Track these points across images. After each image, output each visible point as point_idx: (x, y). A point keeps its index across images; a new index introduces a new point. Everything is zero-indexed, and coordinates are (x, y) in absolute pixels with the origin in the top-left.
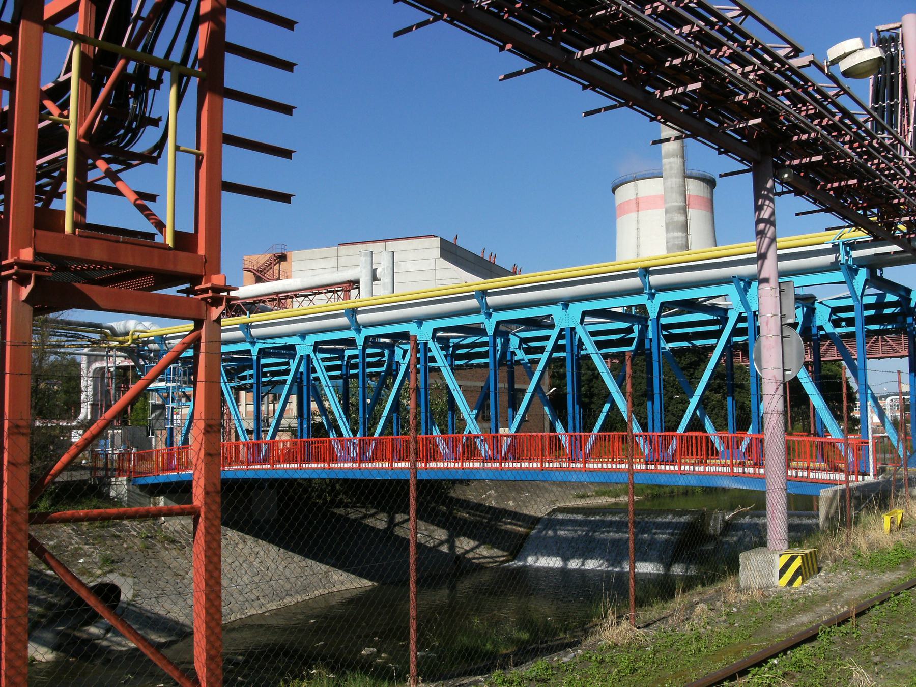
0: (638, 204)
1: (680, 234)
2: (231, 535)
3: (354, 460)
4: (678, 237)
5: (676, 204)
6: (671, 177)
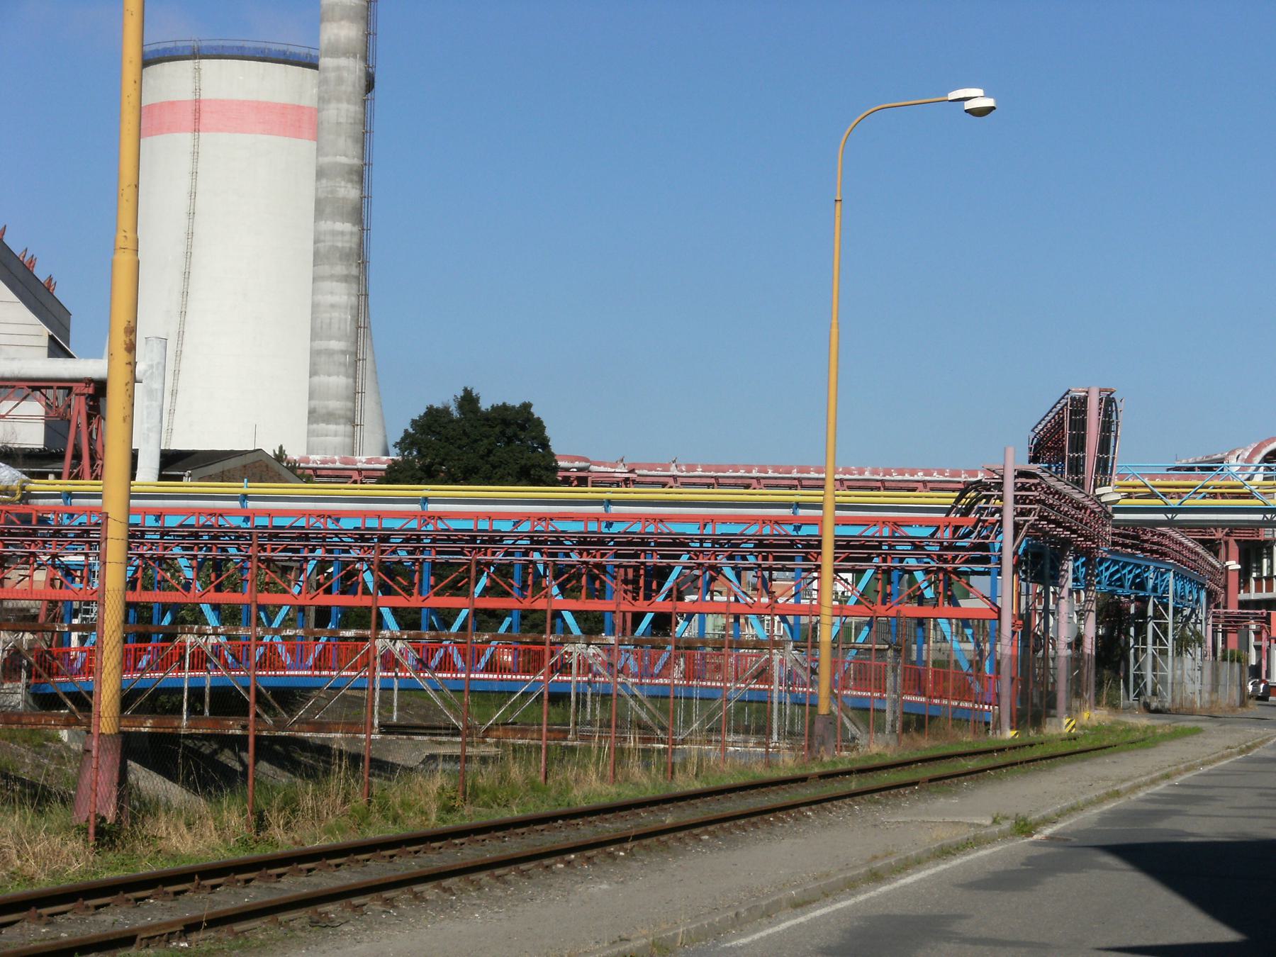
0: (197, 115)
1: (348, 227)
2: (132, 765)
3: (310, 668)
4: (342, 233)
5: (343, 160)
6: (339, 100)
